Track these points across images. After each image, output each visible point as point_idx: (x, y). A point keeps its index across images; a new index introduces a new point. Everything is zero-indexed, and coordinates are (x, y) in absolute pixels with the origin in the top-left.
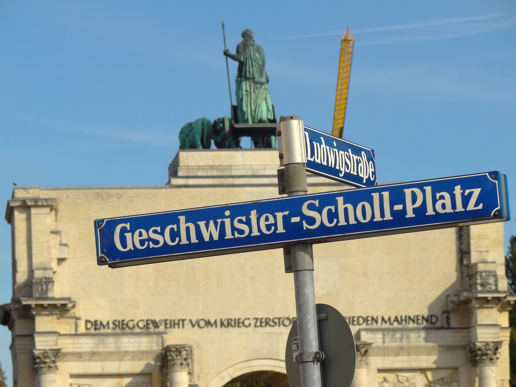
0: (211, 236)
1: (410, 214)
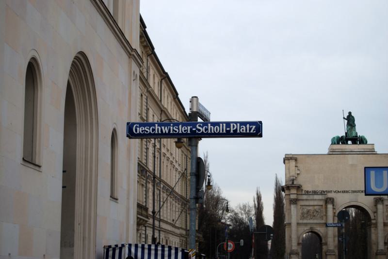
0: (165, 132)
1: (232, 132)
